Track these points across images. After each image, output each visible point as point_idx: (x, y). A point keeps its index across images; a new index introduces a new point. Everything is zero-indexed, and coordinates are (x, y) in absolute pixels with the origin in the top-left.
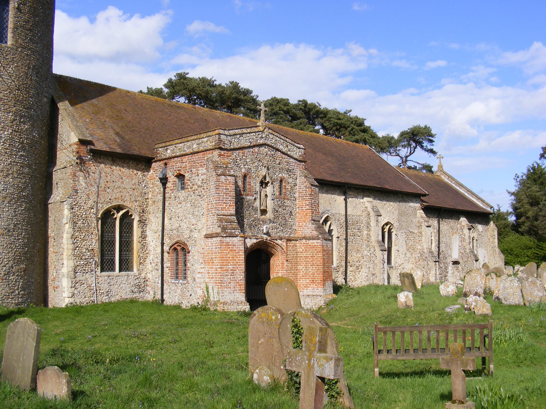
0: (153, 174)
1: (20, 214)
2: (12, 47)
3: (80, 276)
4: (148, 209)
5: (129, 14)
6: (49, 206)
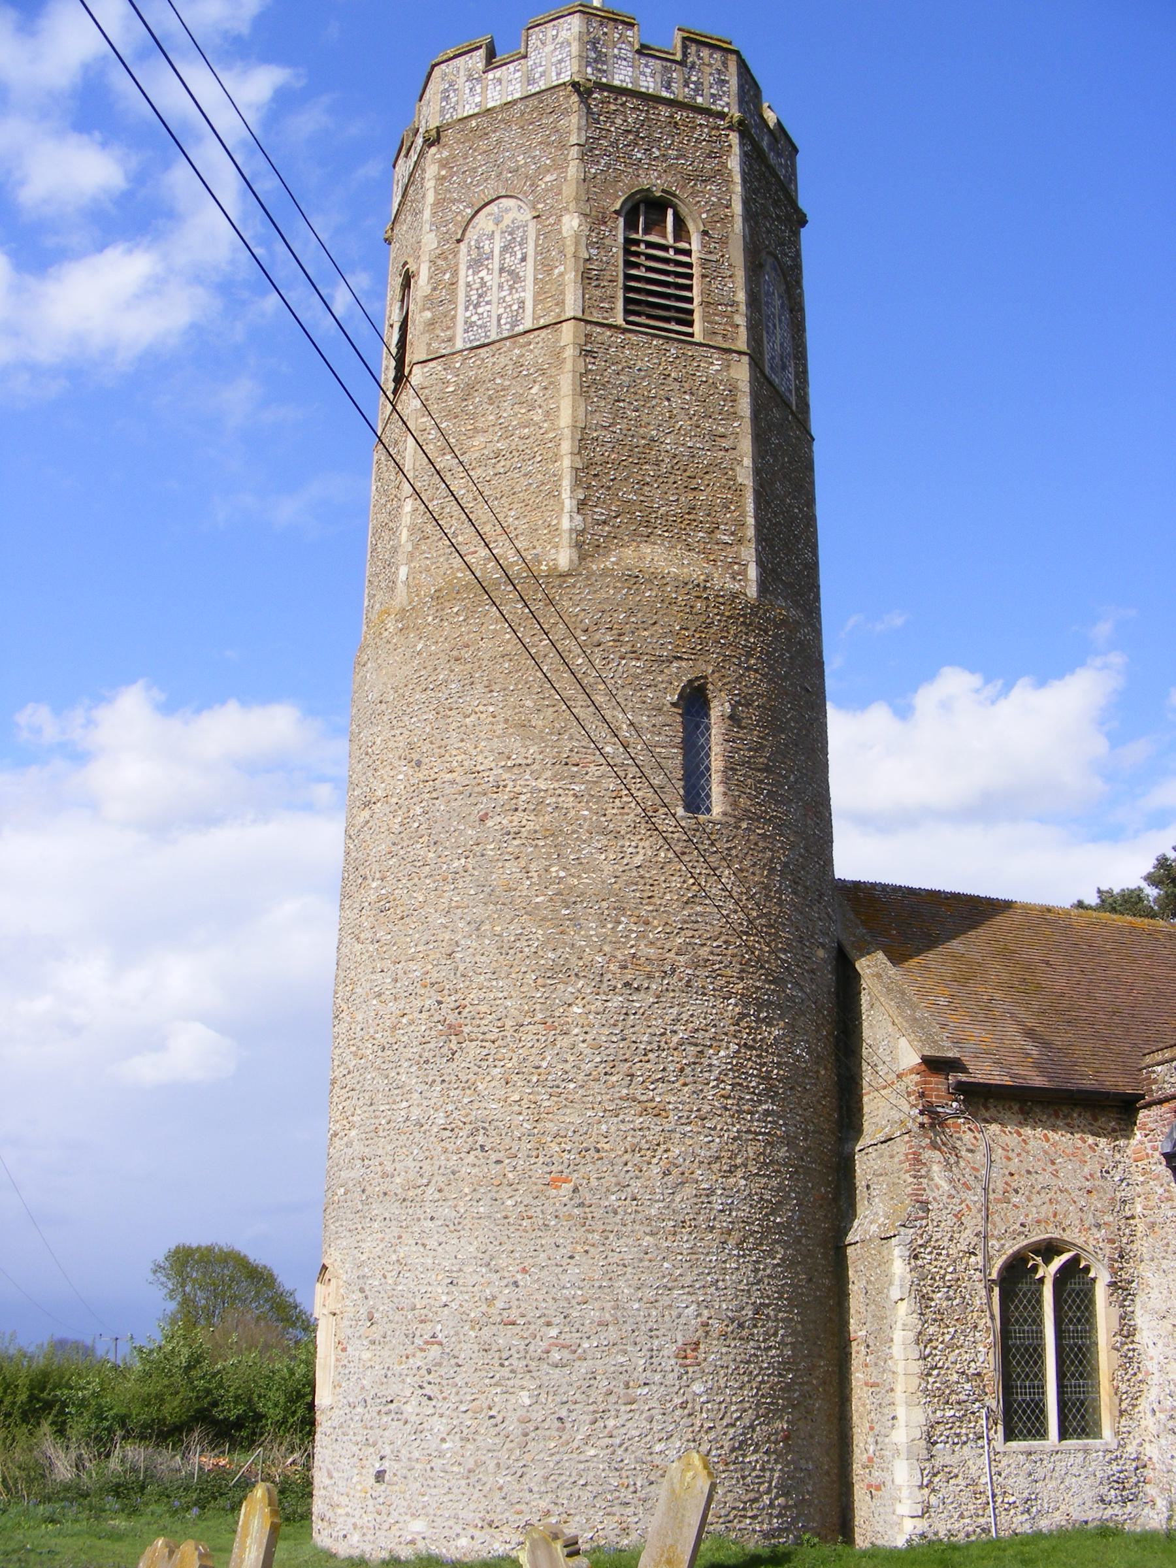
0: (1142, 1143)
1: (769, 1276)
2: (725, 819)
3: (944, 1455)
4: (1134, 1247)
5: (1000, 682)
6: (849, 1250)
